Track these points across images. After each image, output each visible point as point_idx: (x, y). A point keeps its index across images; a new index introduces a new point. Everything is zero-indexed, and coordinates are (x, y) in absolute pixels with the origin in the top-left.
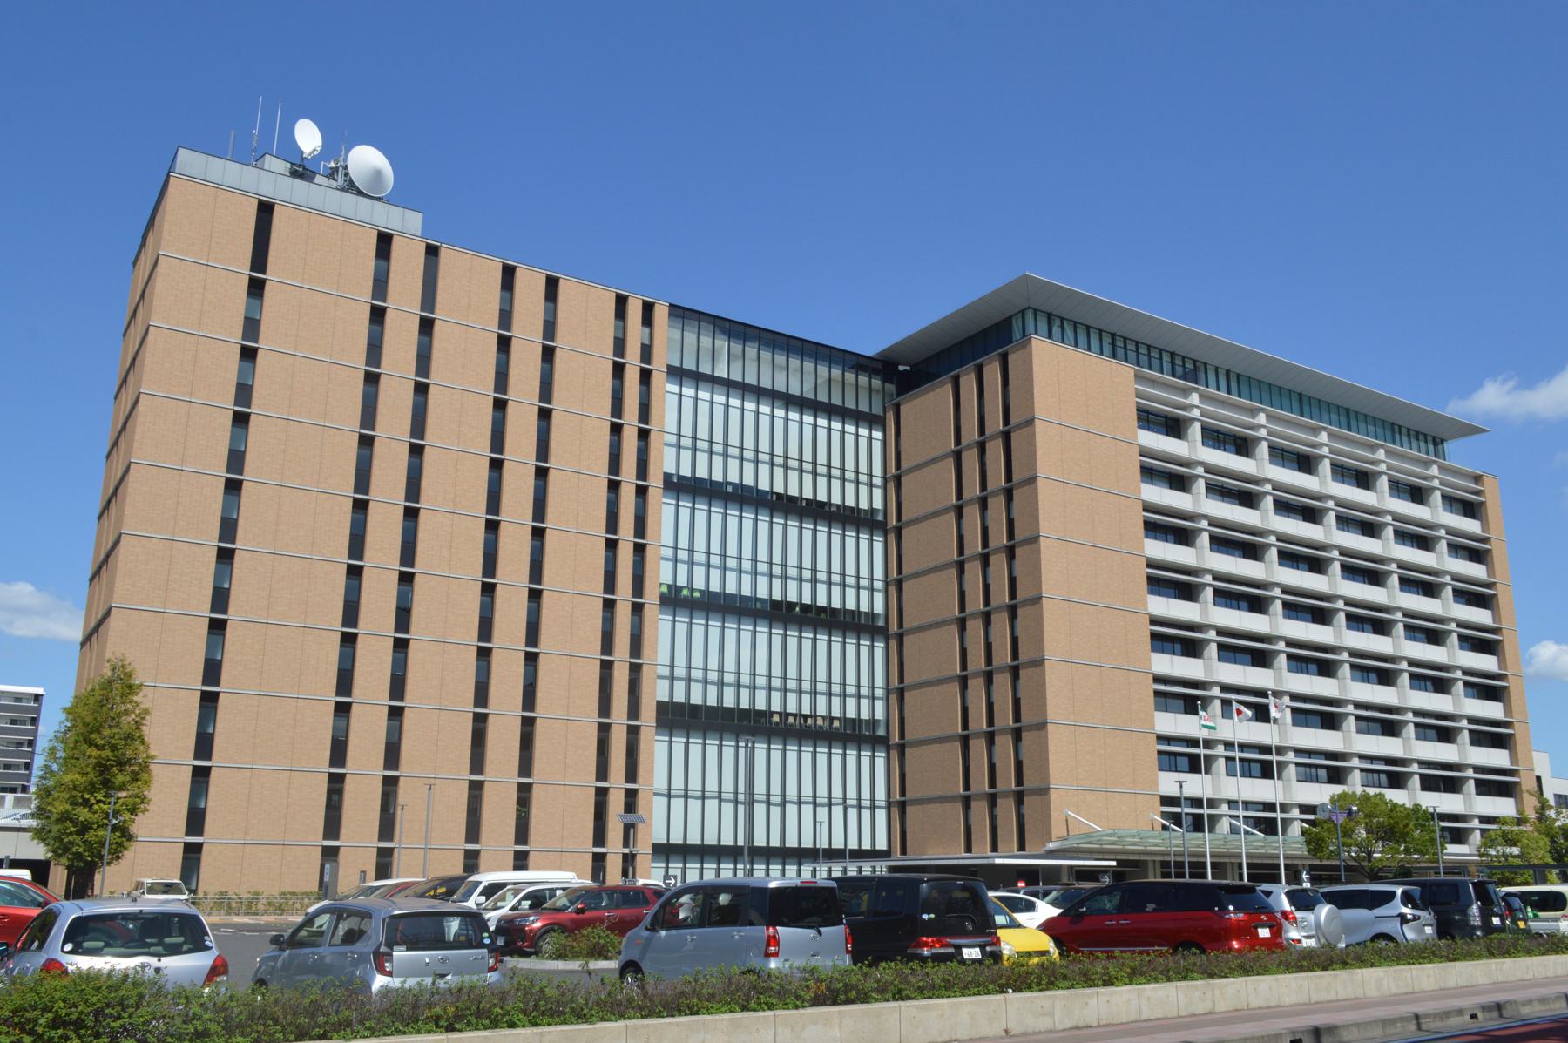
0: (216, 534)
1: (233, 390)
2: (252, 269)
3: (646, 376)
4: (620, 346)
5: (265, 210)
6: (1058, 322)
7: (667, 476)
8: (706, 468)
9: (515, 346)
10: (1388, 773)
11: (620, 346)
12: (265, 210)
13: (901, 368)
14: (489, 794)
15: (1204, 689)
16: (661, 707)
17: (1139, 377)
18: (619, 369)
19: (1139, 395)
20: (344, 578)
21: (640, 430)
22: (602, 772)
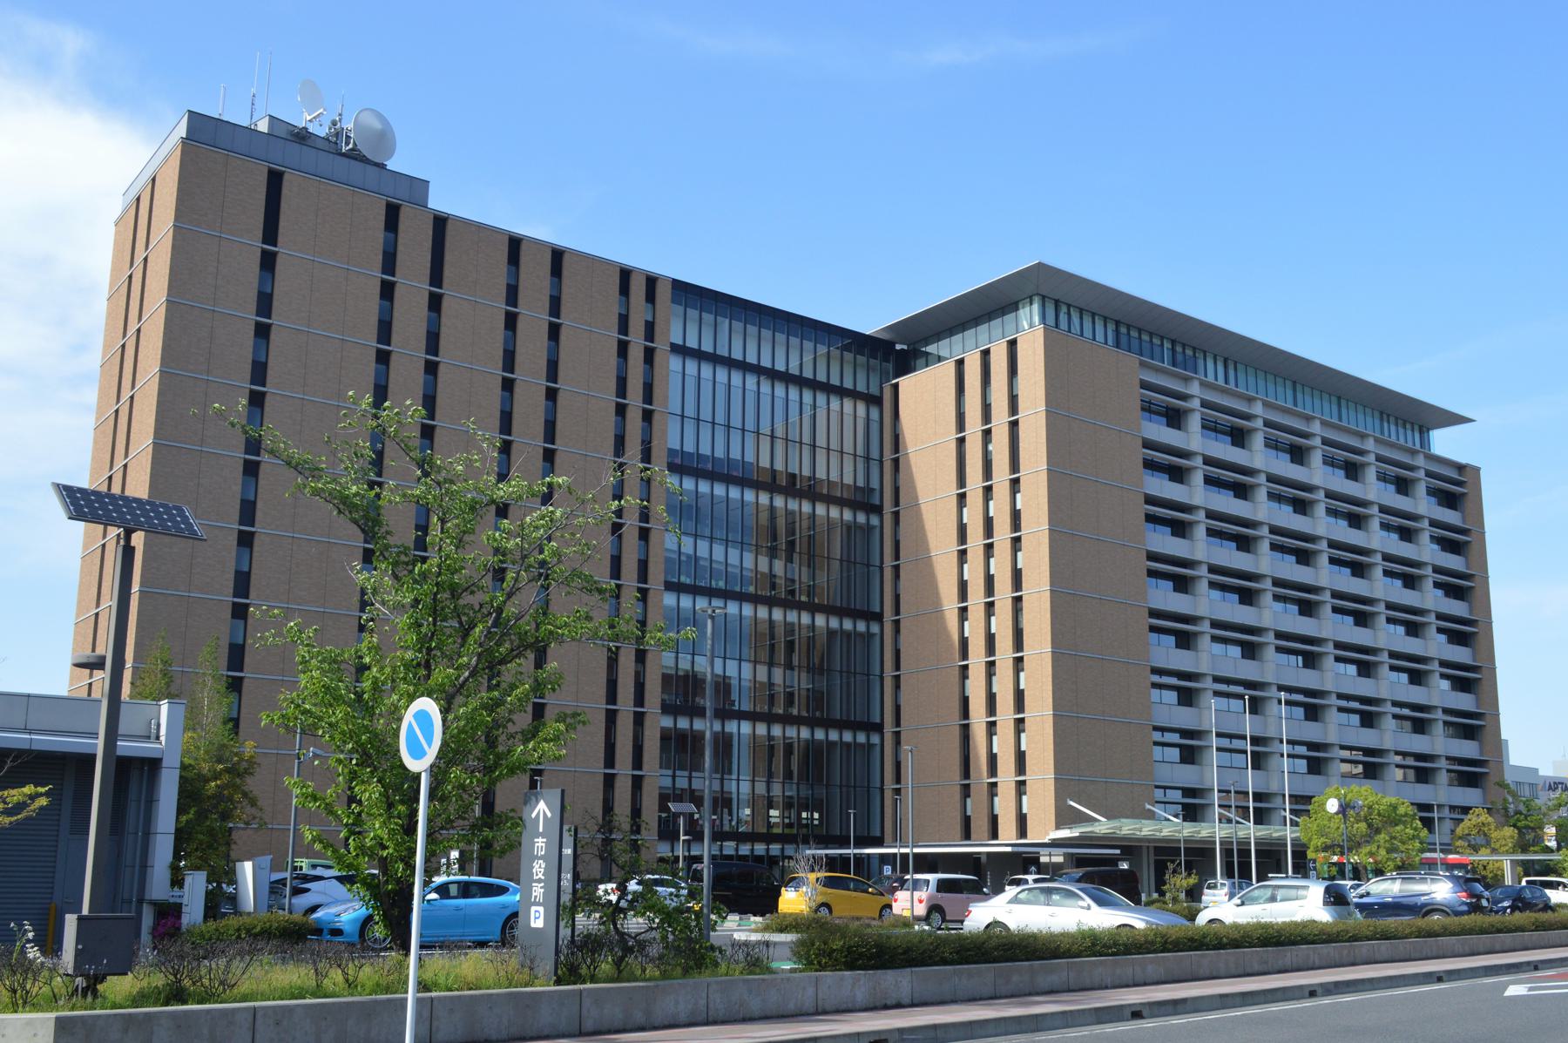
0: (236, 517)
1: (248, 367)
2: (252, 383)
3: (649, 355)
4: (624, 324)
5: (275, 180)
6: (1064, 309)
7: (671, 452)
8: (708, 445)
9: (521, 325)
10: (1417, 769)
11: (624, 324)
12: (275, 180)
13: (898, 347)
14: (539, 428)
15: (1194, 797)
16: (666, 679)
17: (1142, 364)
18: (623, 348)
19: (1145, 385)
20: (373, 365)
21: (644, 410)
22: (610, 761)
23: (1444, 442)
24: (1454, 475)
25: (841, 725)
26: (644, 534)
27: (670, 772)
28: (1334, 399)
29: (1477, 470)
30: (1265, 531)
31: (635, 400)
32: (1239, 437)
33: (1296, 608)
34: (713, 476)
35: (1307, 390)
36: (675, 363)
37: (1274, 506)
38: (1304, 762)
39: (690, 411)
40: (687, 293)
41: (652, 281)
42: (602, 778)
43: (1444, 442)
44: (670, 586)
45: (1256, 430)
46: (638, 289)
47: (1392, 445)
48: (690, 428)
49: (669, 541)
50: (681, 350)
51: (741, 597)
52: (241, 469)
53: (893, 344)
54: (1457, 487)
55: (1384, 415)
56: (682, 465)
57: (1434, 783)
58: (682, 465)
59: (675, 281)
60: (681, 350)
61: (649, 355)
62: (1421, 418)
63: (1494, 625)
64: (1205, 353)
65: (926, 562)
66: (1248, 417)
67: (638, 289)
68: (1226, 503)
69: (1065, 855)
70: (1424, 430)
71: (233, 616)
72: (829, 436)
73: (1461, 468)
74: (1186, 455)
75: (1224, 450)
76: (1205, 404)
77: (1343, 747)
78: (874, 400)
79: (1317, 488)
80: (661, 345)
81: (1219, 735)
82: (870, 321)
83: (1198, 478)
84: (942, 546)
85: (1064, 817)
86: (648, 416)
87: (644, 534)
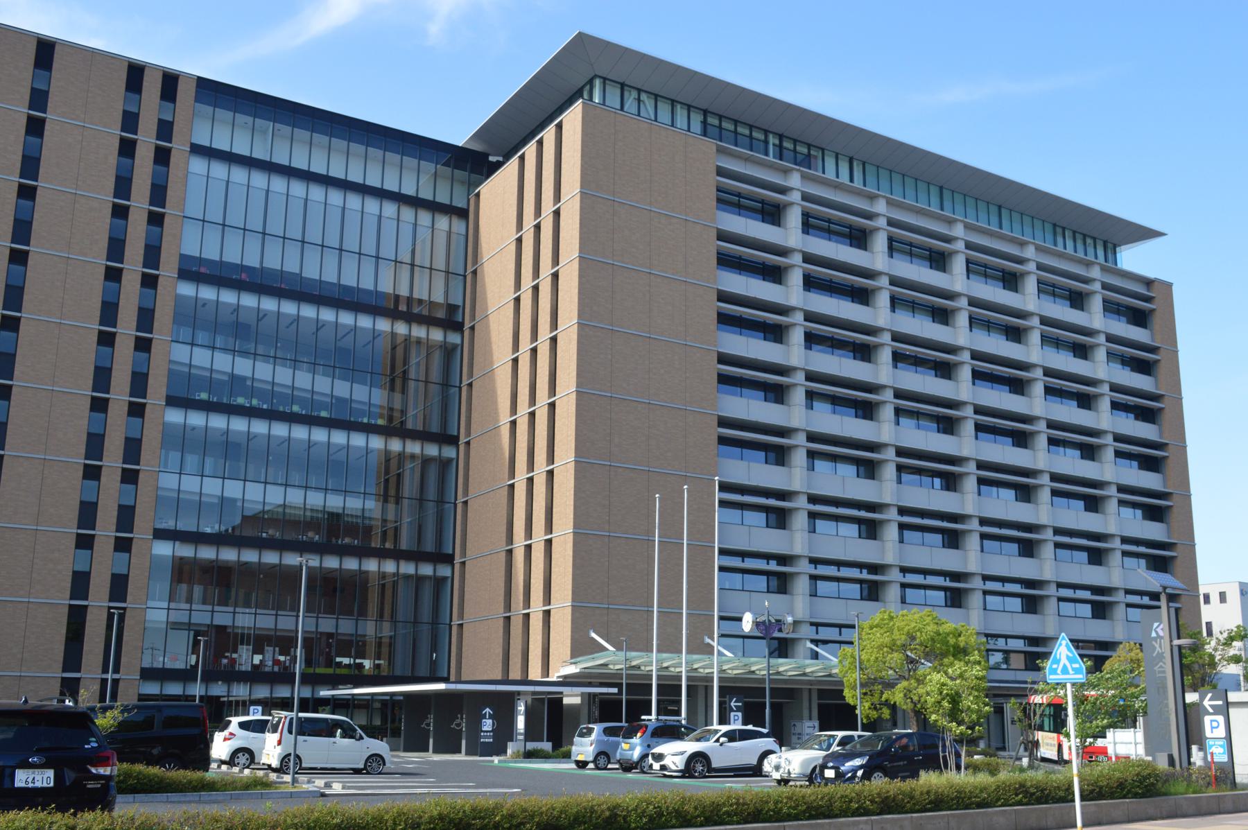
3: (162, 157)
4: (130, 121)
6: (1059, 230)
7: (184, 258)
8: (238, 252)
11: (130, 121)
23: (1132, 259)
24: (1141, 290)
25: (382, 554)
26: (143, 345)
27: (209, 608)
28: (994, 209)
29: (1169, 286)
30: (1038, 373)
31: (140, 203)
32: (1077, 300)
33: (1078, 453)
34: (239, 286)
35: (1016, 216)
36: (198, 165)
37: (897, 317)
38: (1089, 607)
39: (370, 248)
40: (216, 94)
41: (170, 81)
42: (66, 610)
43: (1132, 259)
44: (172, 401)
45: (1029, 273)
46: (151, 87)
47: (1061, 256)
48: (405, 272)
49: (177, 353)
50: (197, 150)
51: (369, 429)
52: (133, 345)
53: (487, 155)
54: (1143, 305)
55: (1058, 228)
56: (192, 271)
57: (1112, 619)
58: (192, 271)
59: (200, 79)
60: (197, 150)
61: (162, 157)
62: (1109, 233)
63: (1189, 450)
64: (1064, 229)
65: (490, 374)
66: (948, 240)
67: (151, 87)
68: (1065, 362)
69: (582, 695)
70: (1111, 248)
71: (123, 481)
72: (372, 244)
73: (1149, 283)
74: (951, 296)
75: (1062, 311)
76: (969, 246)
77: (1128, 592)
78: (463, 213)
79: (1098, 332)
80: (178, 146)
81: (723, 552)
82: (459, 134)
83: (1035, 337)
84: (501, 355)
85: (581, 647)
86: (156, 220)
87: (143, 345)
